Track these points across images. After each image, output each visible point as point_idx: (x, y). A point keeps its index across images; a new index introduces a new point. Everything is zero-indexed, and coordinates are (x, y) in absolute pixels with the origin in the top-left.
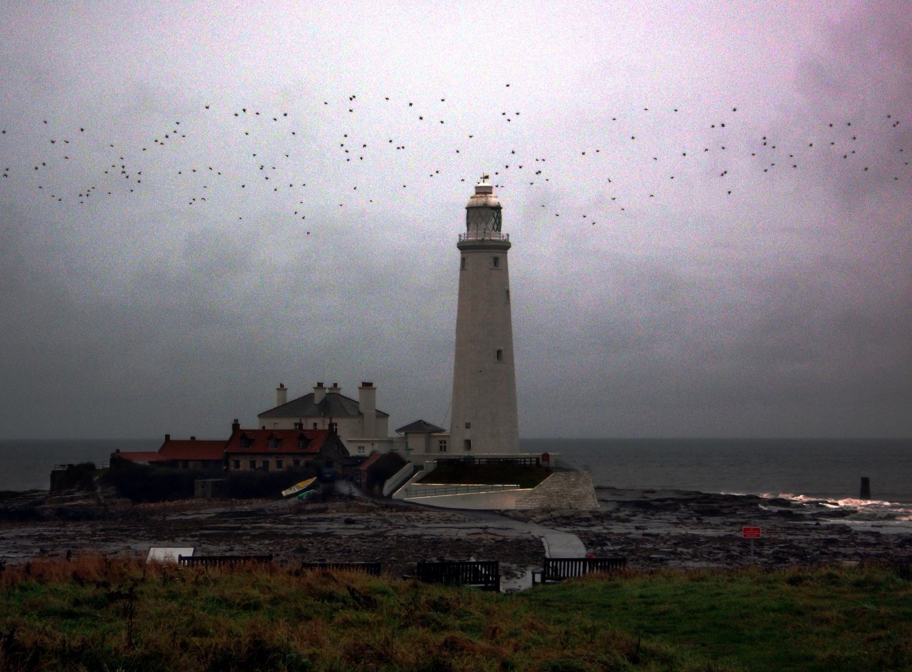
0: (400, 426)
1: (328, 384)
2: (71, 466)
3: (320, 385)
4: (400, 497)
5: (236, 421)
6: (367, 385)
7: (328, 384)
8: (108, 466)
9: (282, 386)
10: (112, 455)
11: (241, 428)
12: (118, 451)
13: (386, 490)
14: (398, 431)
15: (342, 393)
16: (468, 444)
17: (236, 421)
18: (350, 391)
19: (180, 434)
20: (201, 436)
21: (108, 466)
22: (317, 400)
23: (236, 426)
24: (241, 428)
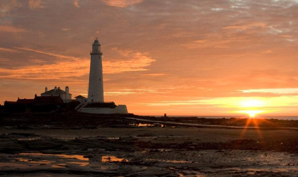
0: (75, 96)
1: (57, 87)
2: (284, 120)
3: (56, 87)
4: (79, 111)
5: (36, 94)
6: (67, 87)
7: (57, 87)
8: (102, 161)
9: (46, 87)
10: (5, 102)
11: (37, 96)
12: (6, 101)
13: (76, 109)
14: (75, 98)
15: (61, 89)
16: (92, 100)
17: (36, 94)
18: (63, 89)
19: (22, 98)
20: (26, 98)
21: (102, 161)
22: (55, 91)
23: (36, 95)
24: (37, 96)
